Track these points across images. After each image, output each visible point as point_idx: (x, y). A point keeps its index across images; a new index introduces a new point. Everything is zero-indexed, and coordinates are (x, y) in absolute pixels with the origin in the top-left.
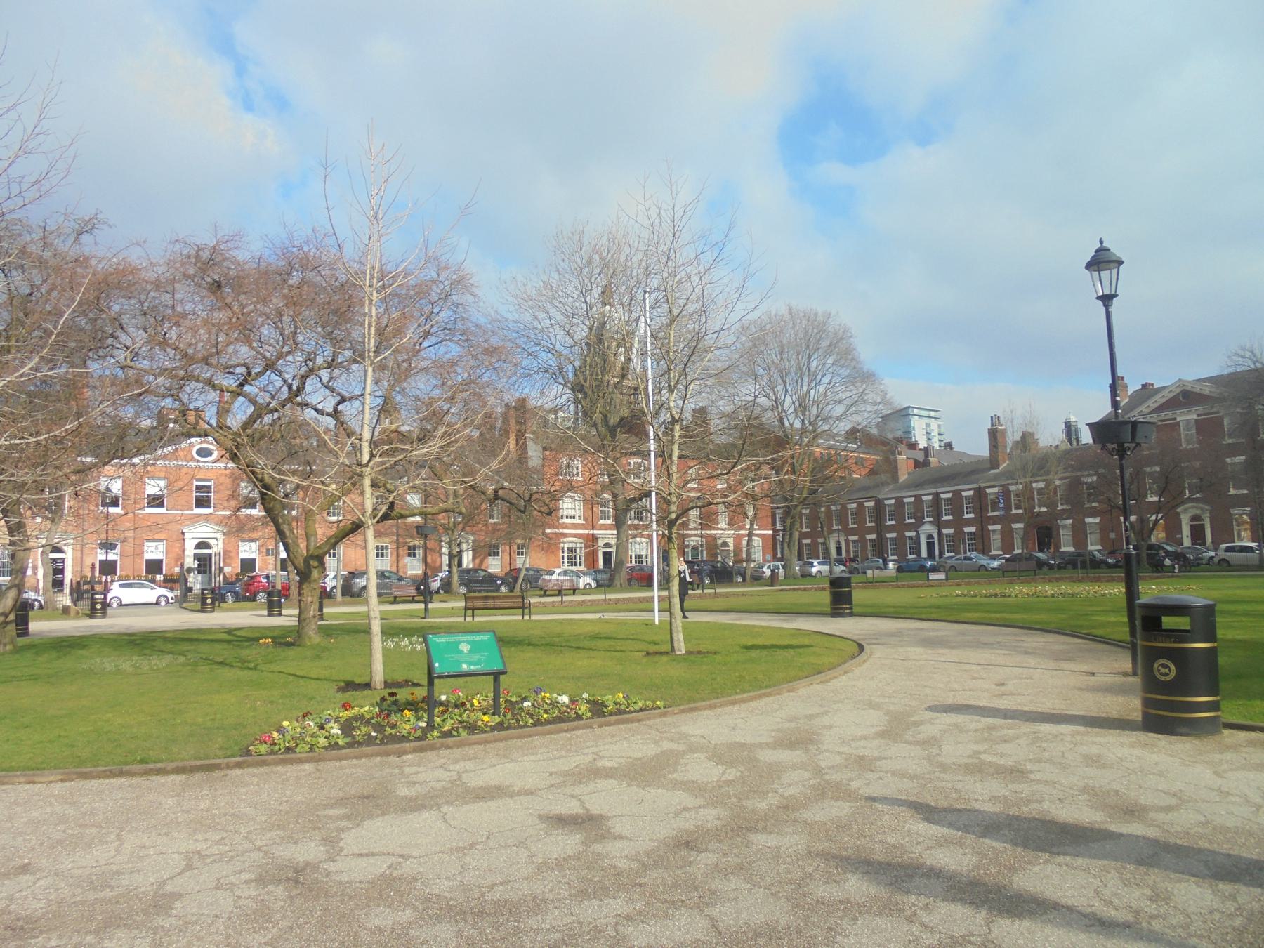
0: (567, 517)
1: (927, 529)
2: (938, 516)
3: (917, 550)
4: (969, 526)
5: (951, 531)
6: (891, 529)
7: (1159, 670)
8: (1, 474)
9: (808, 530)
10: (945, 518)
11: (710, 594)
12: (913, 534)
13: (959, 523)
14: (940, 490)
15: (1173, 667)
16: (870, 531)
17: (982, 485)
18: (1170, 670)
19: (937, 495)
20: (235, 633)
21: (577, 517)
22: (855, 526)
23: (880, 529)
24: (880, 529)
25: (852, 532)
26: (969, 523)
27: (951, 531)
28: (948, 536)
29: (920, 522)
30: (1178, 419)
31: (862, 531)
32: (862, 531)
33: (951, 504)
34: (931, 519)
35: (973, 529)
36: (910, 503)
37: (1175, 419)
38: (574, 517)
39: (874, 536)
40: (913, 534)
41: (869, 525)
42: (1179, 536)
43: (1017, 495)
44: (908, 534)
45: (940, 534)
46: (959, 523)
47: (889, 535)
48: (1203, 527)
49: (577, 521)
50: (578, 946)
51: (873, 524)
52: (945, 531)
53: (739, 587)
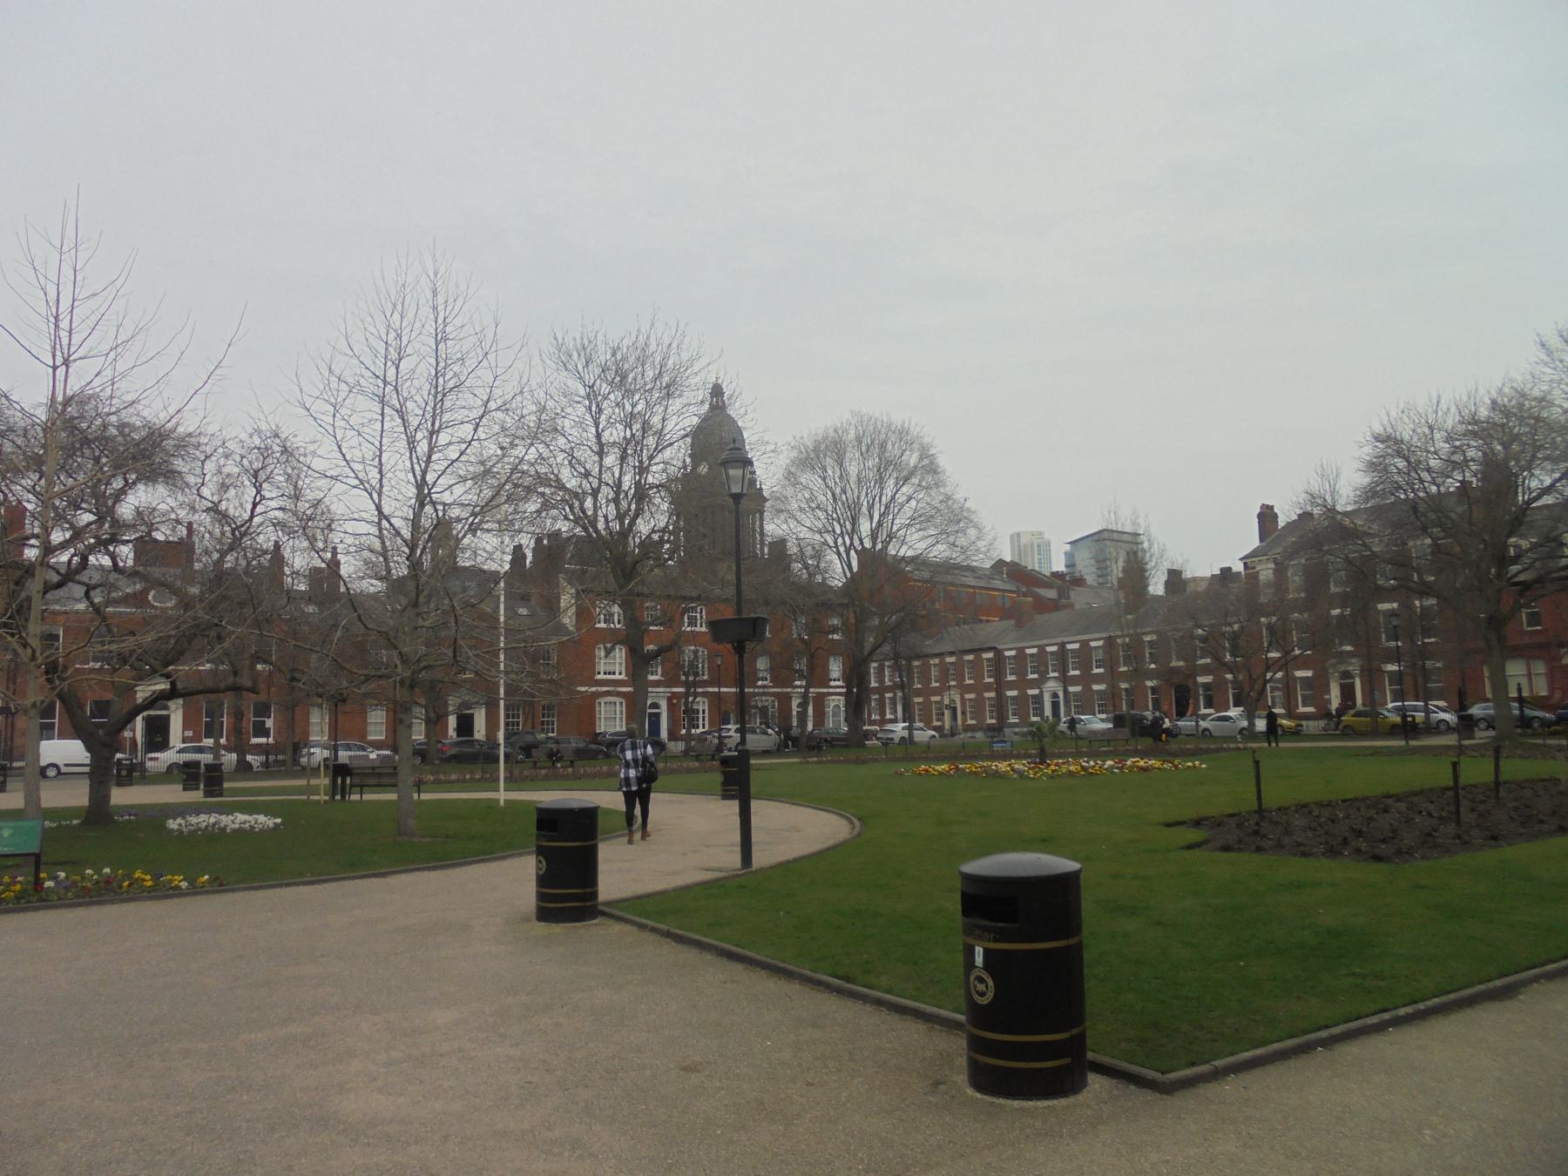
0: (605, 673)
1: (1052, 686)
2: (1063, 671)
3: (1039, 711)
4: (1098, 683)
5: (1078, 689)
6: (1012, 686)
7: (975, 987)
8: (1567, 468)
9: (937, 685)
10: (1072, 673)
12: (1036, 692)
13: (1087, 679)
14: (1066, 640)
15: (990, 982)
16: (988, 687)
17: (1112, 634)
18: (987, 987)
19: (1062, 645)
21: (617, 673)
22: (972, 682)
23: (1000, 686)
24: (1000, 686)
25: (969, 689)
26: (1098, 679)
27: (1078, 689)
28: (1075, 694)
29: (1043, 678)
30: (1258, 569)
31: (979, 688)
32: (979, 688)
33: (1078, 657)
34: (1056, 674)
35: (1102, 687)
37: (1254, 568)
38: (614, 673)
39: (992, 694)
40: (1036, 692)
41: (988, 680)
42: (1327, 697)
43: (1151, 647)
44: (1030, 692)
45: (1066, 692)
46: (1087, 679)
47: (1010, 693)
48: (1352, 686)
49: (617, 677)
51: (992, 680)
52: (1071, 689)
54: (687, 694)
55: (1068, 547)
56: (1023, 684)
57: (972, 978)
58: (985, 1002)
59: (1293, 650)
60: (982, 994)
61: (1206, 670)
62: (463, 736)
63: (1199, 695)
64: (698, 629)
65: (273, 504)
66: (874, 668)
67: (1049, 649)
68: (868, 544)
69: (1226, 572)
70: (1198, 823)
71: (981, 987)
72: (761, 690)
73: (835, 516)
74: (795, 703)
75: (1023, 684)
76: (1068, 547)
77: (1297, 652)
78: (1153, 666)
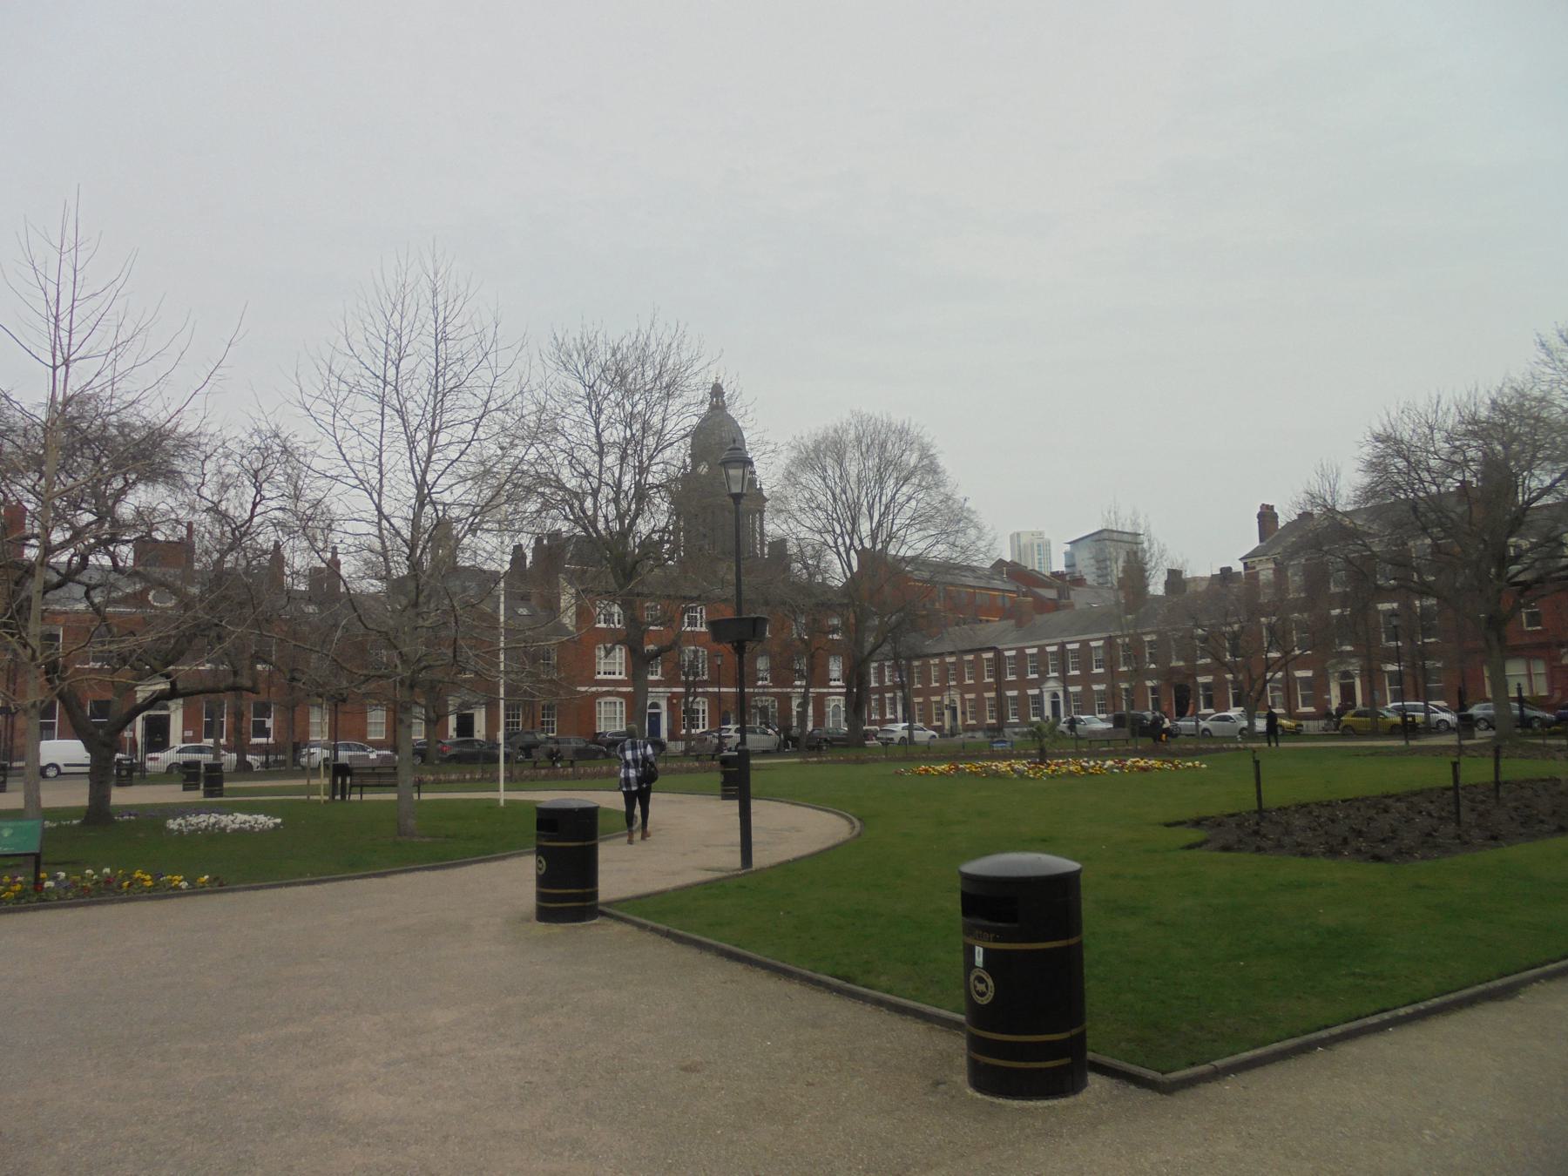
0: (605, 673)
1: (1052, 686)
2: (1063, 671)
3: (1039, 711)
4: (1098, 683)
5: (1078, 689)
6: (1012, 686)
7: (975, 987)
9: (937, 685)
10: (1072, 673)
11: (260, 745)
12: (1036, 692)
13: (1087, 679)
14: (1066, 640)
15: (990, 982)
16: (988, 687)
17: (1112, 634)
18: (987, 987)
19: (1062, 645)
20: (377, 501)
21: (617, 673)
22: (972, 682)
23: (1000, 686)
24: (1000, 686)
25: (969, 689)
26: (1098, 679)
27: (1078, 689)
28: (1075, 694)
29: (1043, 678)
30: (1258, 569)
31: (979, 688)
32: (979, 688)
33: (1078, 657)
34: (1056, 674)
35: (1102, 687)
36: (1098, 647)
37: (1254, 568)
38: (614, 673)
39: (992, 694)
40: (1036, 692)
41: (988, 680)
42: (1327, 697)
43: (1151, 647)
44: (1030, 692)
45: (1066, 692)
46: (1087, 679)
47: (1010, 693)
48: (1352, 686)
49: (617, 677)
50: (3, 479)
51: (992, 680)
52: (1071, 689)
53: (789, 757)
54: (687, 694)
55: (1068, 547)
56: (1023, 684)
57: (972, 978)
58: (985, 1002)
59: (1293, 650)
60: (982, 994)
61: (1206, 670)
62: (463, 736)
63: (1199, 695)
64: (698, 629)
65: (273, 504)
66: (874, 668)
67: (1049, 649)
68: (868, 544)
69: (1226, 572)
70: (1198, 823)
71: (981, 987)
72: (761, 690)
73: (835, 516)
74: (795, 703)
75: (1023, 684)
76: (1068, 547)
77: (1297, 652)
78: (1153, 666)
